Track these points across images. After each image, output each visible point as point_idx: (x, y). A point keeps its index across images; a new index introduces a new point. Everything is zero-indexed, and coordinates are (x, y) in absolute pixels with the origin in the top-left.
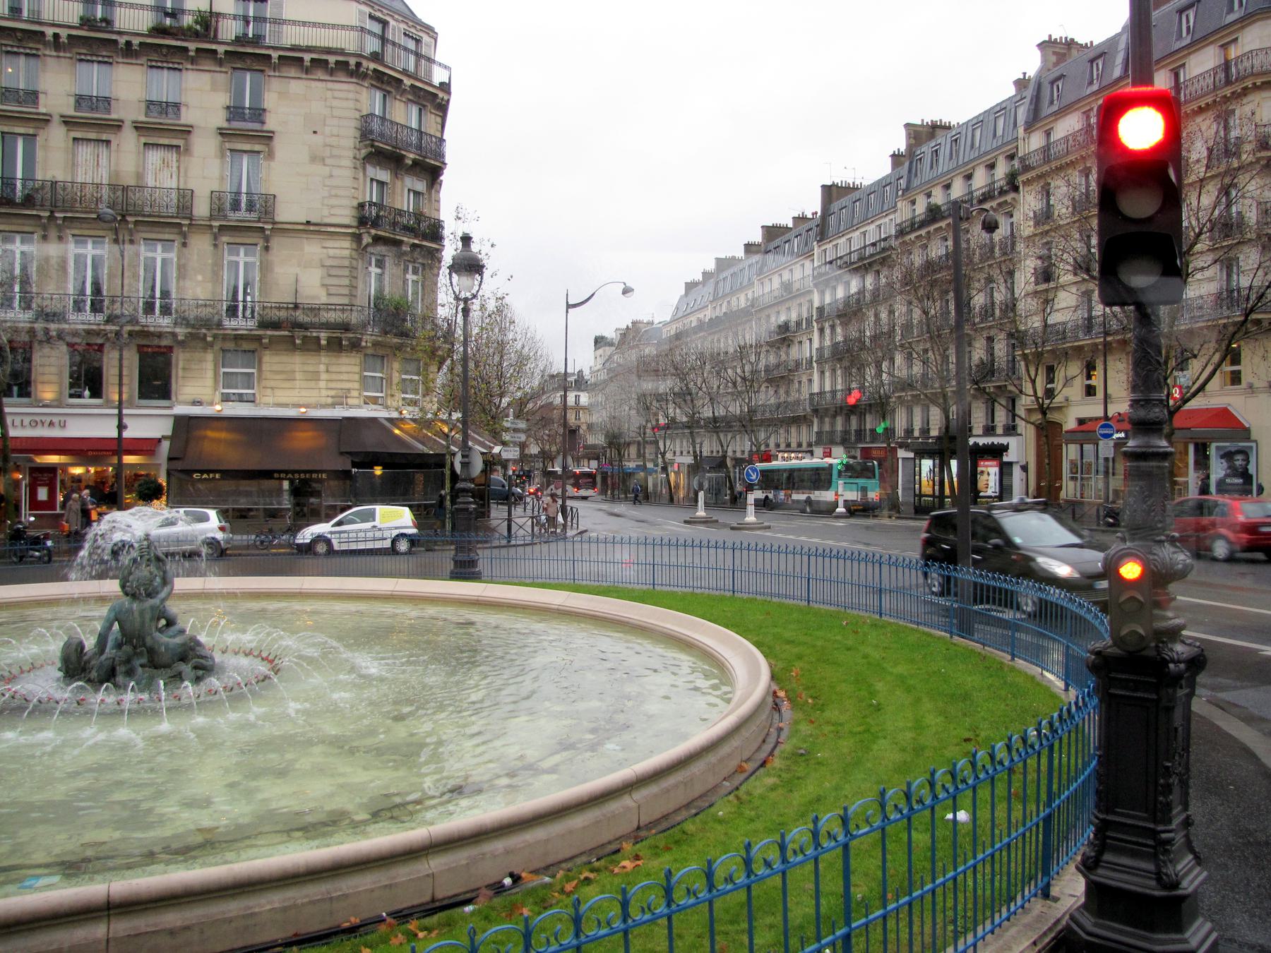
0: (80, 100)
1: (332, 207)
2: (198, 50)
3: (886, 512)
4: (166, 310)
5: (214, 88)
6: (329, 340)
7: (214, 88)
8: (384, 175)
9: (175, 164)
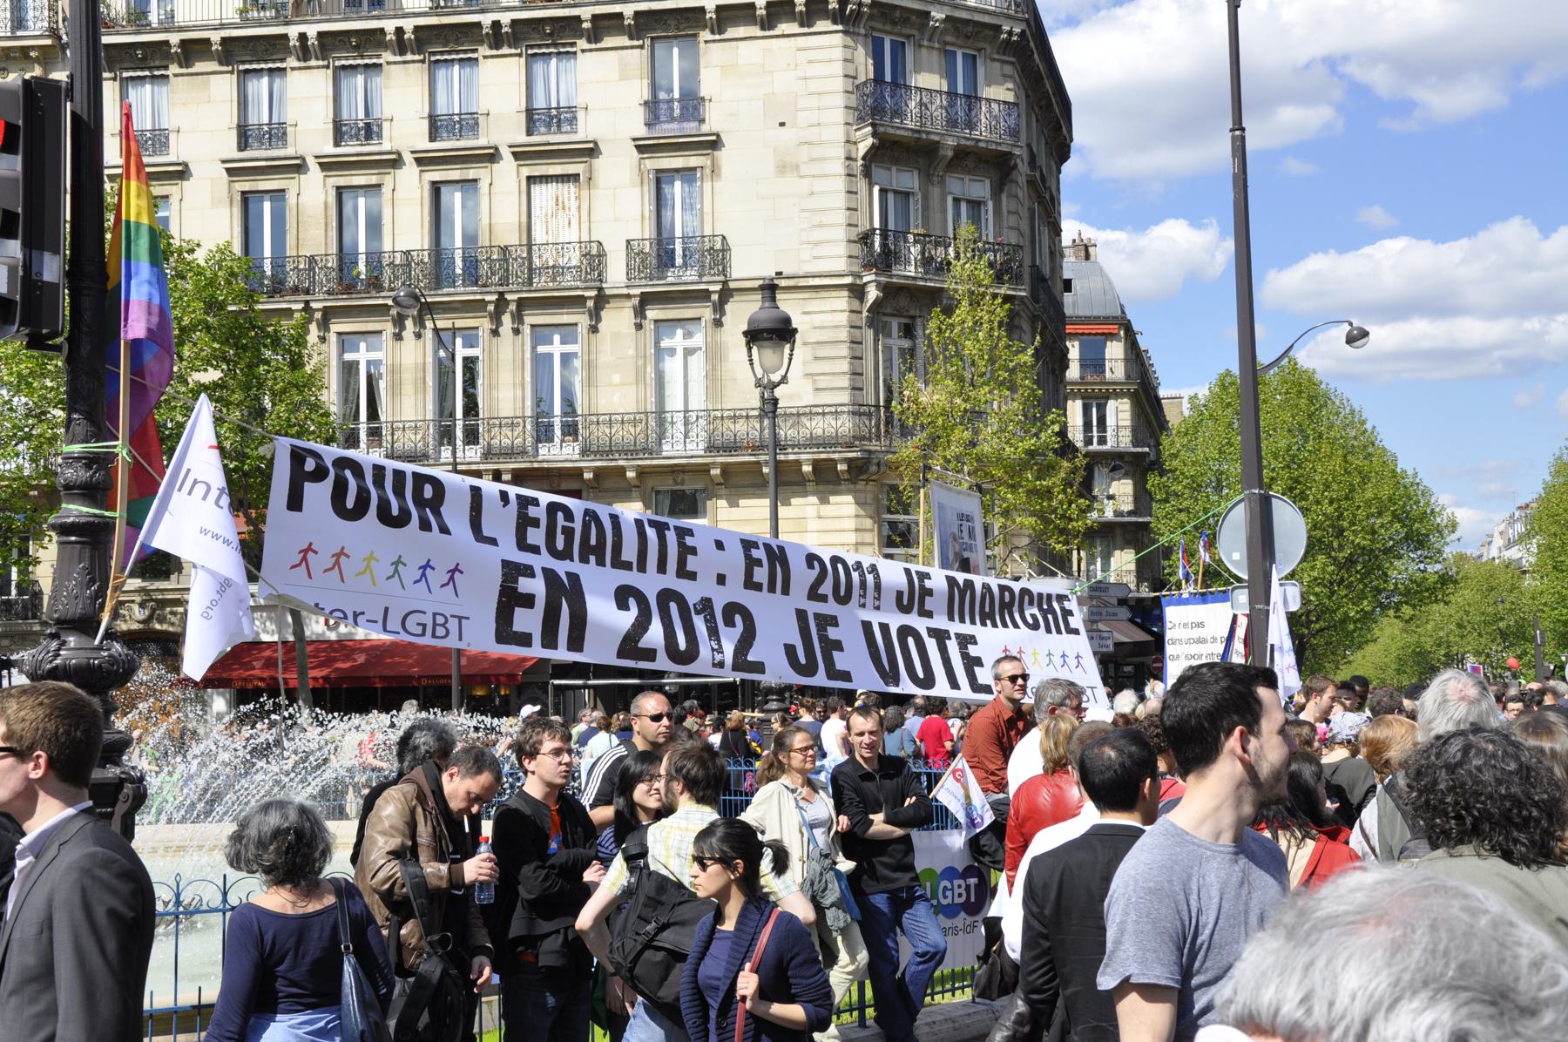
0: (436, 127)
1: (816, 244)
2: (595, 17)
3: (1325, 751)
4: (571, 430)
5: (624, 76)
6: (816, 464)
7: (624, 76)
8: (909, 180)
9: (574, 204)
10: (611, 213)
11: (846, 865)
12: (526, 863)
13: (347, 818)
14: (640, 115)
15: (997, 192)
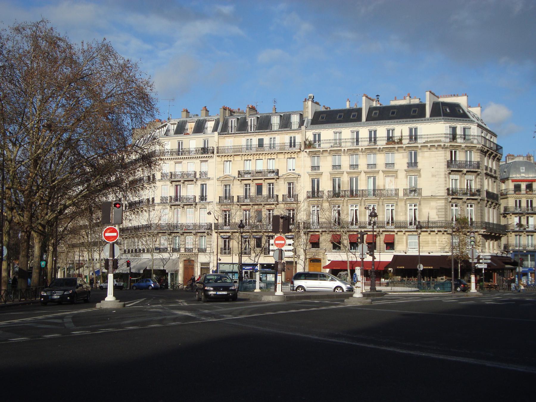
10: (402, 183)
11: (142, 272)
12: (103, 214)
13: (260, 264)
14: (406, 165)
15: (476, 178)
